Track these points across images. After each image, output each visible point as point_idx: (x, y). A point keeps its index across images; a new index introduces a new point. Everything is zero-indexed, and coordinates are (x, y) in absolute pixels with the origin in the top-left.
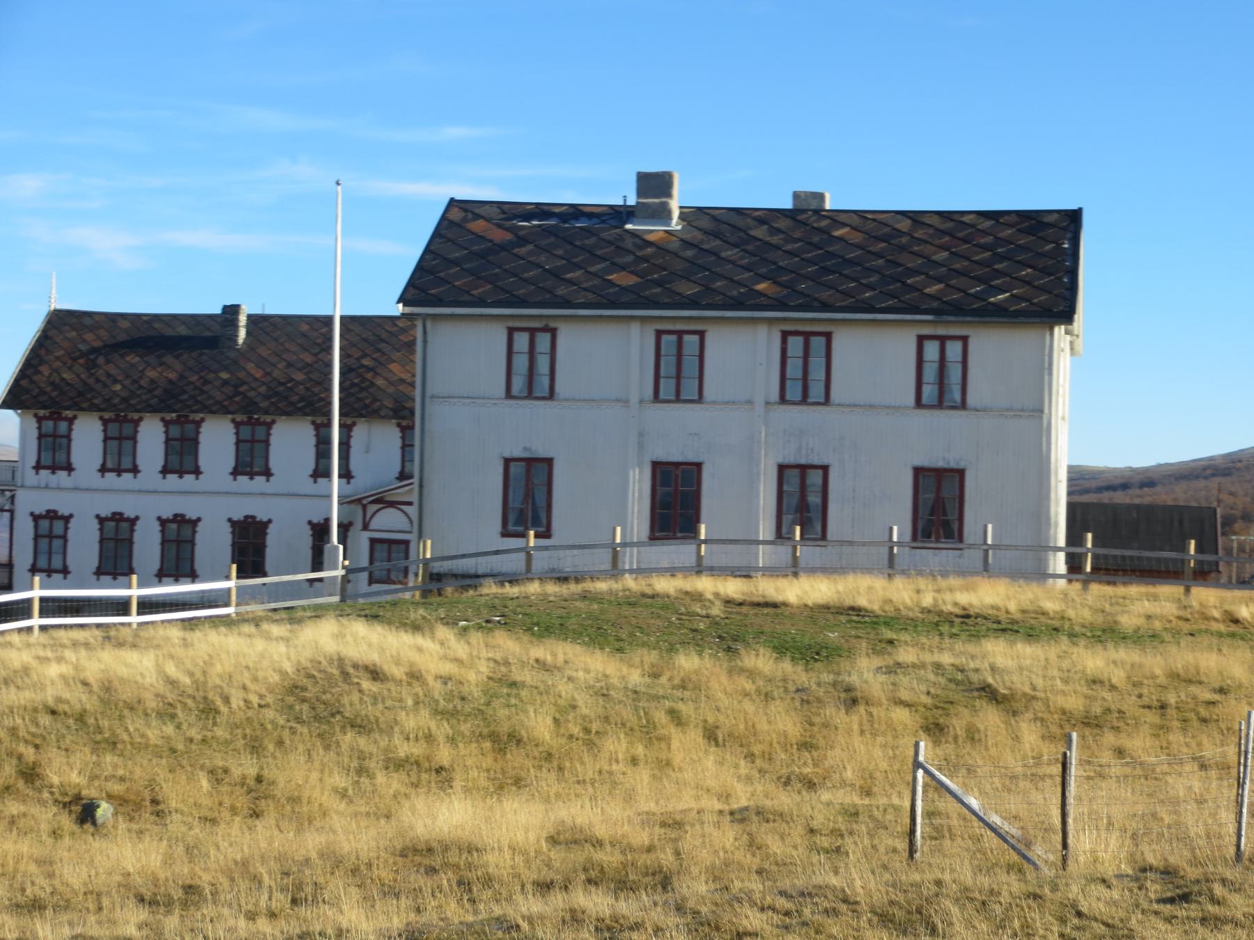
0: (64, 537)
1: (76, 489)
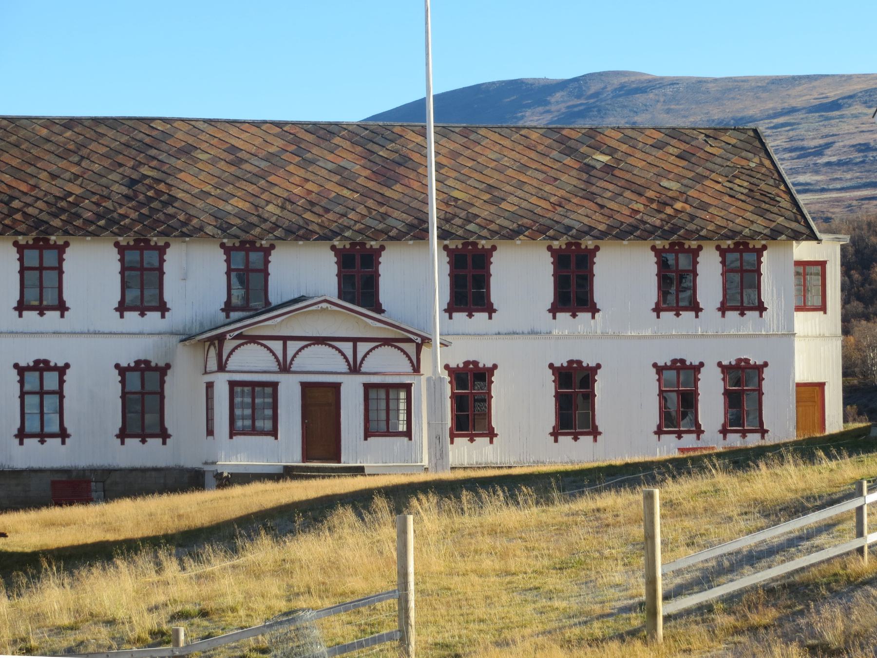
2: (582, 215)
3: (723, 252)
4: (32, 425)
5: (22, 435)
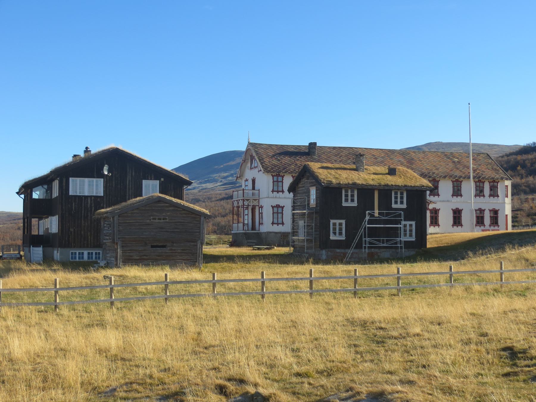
0: (282, 213)
1: (285, 198)
2: (457, 173)
3: (490, 182)
4: (275, 221)
5: (273, 223)
